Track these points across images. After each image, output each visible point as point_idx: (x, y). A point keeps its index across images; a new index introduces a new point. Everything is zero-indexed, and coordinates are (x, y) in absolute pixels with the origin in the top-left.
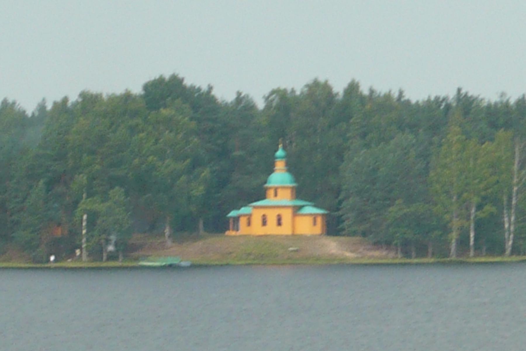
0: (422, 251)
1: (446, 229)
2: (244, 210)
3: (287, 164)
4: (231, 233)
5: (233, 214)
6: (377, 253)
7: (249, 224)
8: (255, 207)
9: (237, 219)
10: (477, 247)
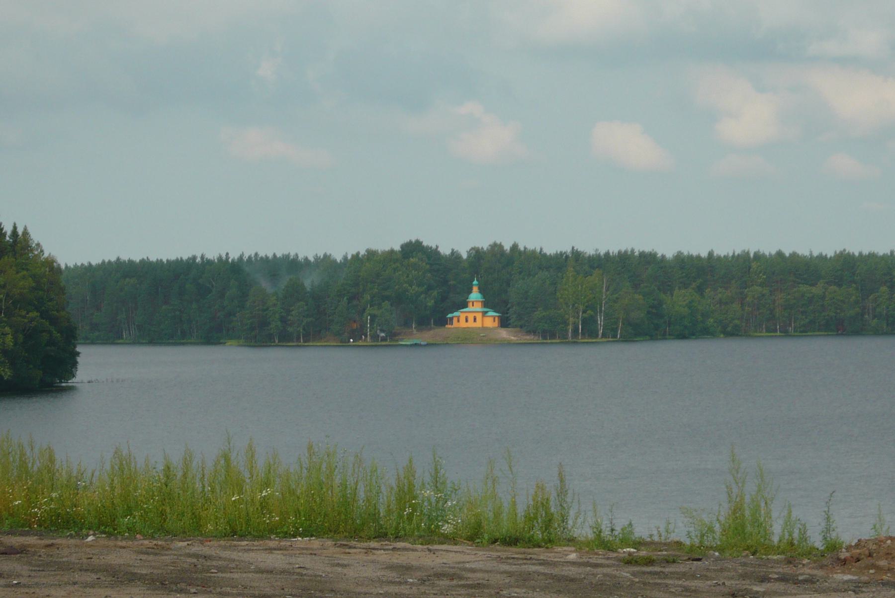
0: (553, 336)
1: (566, 323)
2: (456, 314)
3: (479, 288)
4: (448, 326)
5: (450, 316)
6: (528, 337)
7: (458, 321)
8: (462, 312)
9: (452, 319)
10: (583, 334)
